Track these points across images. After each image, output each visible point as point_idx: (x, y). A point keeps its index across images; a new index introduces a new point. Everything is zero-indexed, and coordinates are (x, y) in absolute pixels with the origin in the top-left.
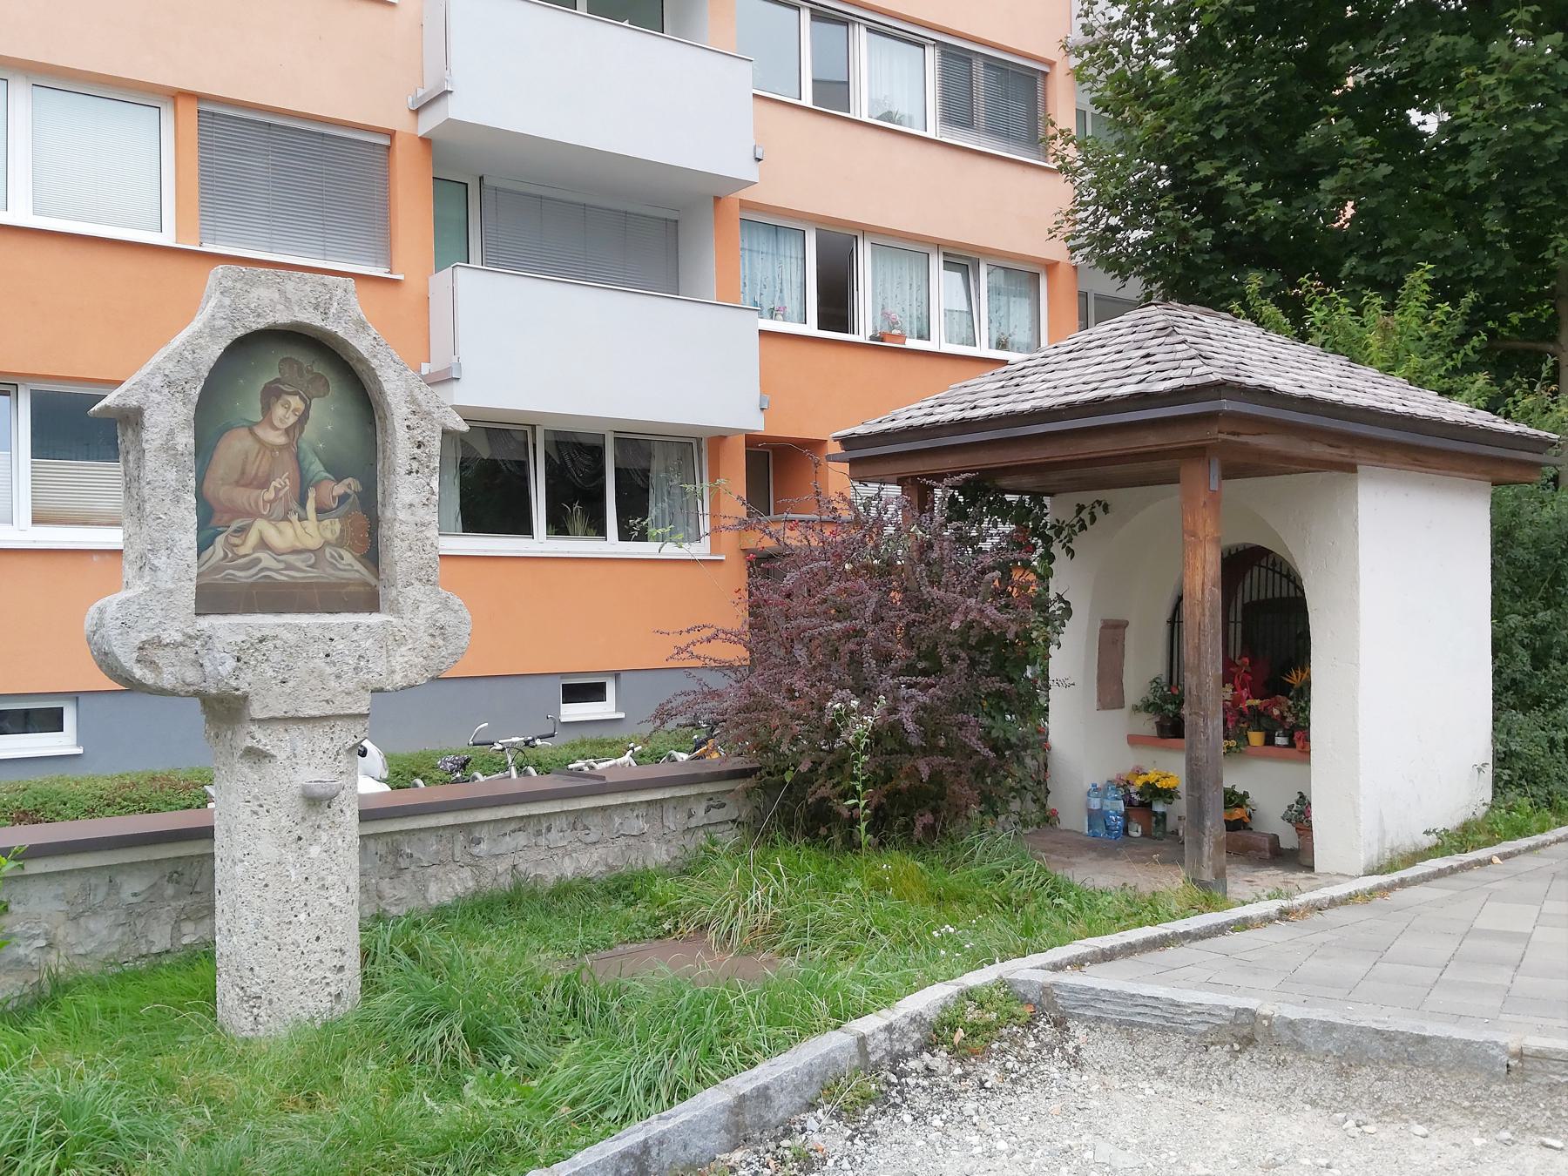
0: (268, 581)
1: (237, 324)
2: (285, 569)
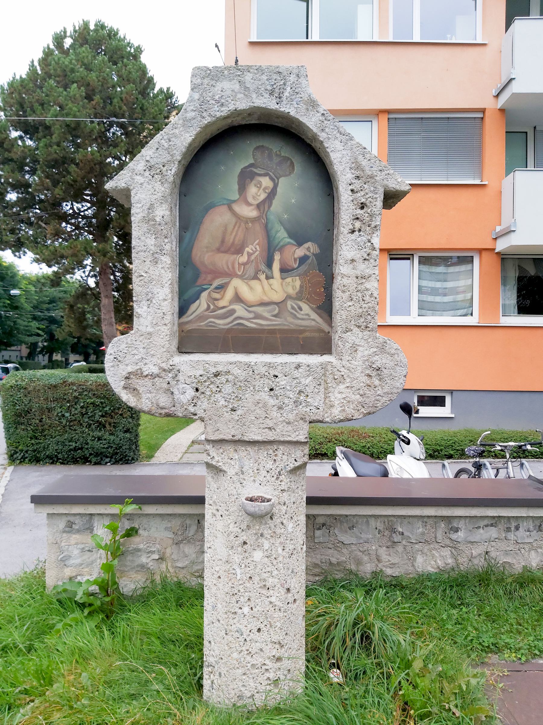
0: (240, 327)
1: (205, 114)
2: (255, 318)
